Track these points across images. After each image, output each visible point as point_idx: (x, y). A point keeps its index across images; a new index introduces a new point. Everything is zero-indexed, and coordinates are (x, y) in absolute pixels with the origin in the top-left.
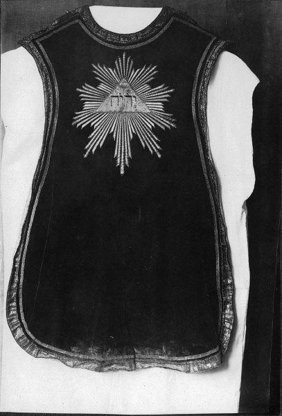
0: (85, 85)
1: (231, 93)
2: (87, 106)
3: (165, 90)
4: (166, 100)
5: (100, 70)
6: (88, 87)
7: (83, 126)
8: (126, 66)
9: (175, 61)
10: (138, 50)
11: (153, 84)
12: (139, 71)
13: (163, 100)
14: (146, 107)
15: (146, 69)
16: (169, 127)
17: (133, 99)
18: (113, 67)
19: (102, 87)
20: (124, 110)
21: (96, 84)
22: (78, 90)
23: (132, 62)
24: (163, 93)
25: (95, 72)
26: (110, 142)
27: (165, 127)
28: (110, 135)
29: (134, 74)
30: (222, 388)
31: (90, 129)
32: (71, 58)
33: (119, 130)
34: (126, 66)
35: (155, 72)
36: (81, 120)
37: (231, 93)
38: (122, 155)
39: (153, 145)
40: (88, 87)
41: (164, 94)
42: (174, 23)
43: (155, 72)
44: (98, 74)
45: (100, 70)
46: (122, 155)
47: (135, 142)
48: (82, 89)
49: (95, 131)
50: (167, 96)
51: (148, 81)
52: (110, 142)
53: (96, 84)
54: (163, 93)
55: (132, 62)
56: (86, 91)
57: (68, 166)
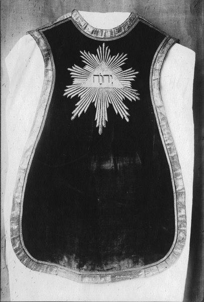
0: (74, 66)
1: (175, 72)
2: (76, 81)
3: (133, 72)
4: (133, 80)
5: (85, 55)
6: (76, 68)
7: (72, 97)
8: (102, 52)
9: (139, 47)
10: (116, 46)
11: (124, 68)
12: (115, 57)
13: (131, 79)
14: (120, 84)
15: (119, 56)
16: (134, 76)
17: (110, 77)
18: (96, 53)
19: (87, 68)
20: (102, 84)
21: (82, 65)
22: (69, 69)
23: (109, 51)
24: (131, 75)
25: (82, 57)
26: (92, 109)
27: (132, 100)
28: (111, 105)
29: (110, 59)
30: (171, 277)
31: (77, 99)
32: (66, 46)
33: (99, 101)
34: (102, 52)
35: (126, 59)
36: (70, 92)
37: (175, 72)
38: (101, 118)
39: (123, 112)
40: (76, 68)
41: (131, 75)
42: (140, 22)
43: (126, 59)
44: (84, 58)
45: (85, 55)
46: (101, 118)
47: (110, 110)
48: (72, 69)
49: (113, 103)
50: (134, 76)
51: (121, 65)
52: (92, 109)
53: (82, 65)
54: (131, 75)
55: (109, 51)
56: (75, 70)
57: (65, 129)
